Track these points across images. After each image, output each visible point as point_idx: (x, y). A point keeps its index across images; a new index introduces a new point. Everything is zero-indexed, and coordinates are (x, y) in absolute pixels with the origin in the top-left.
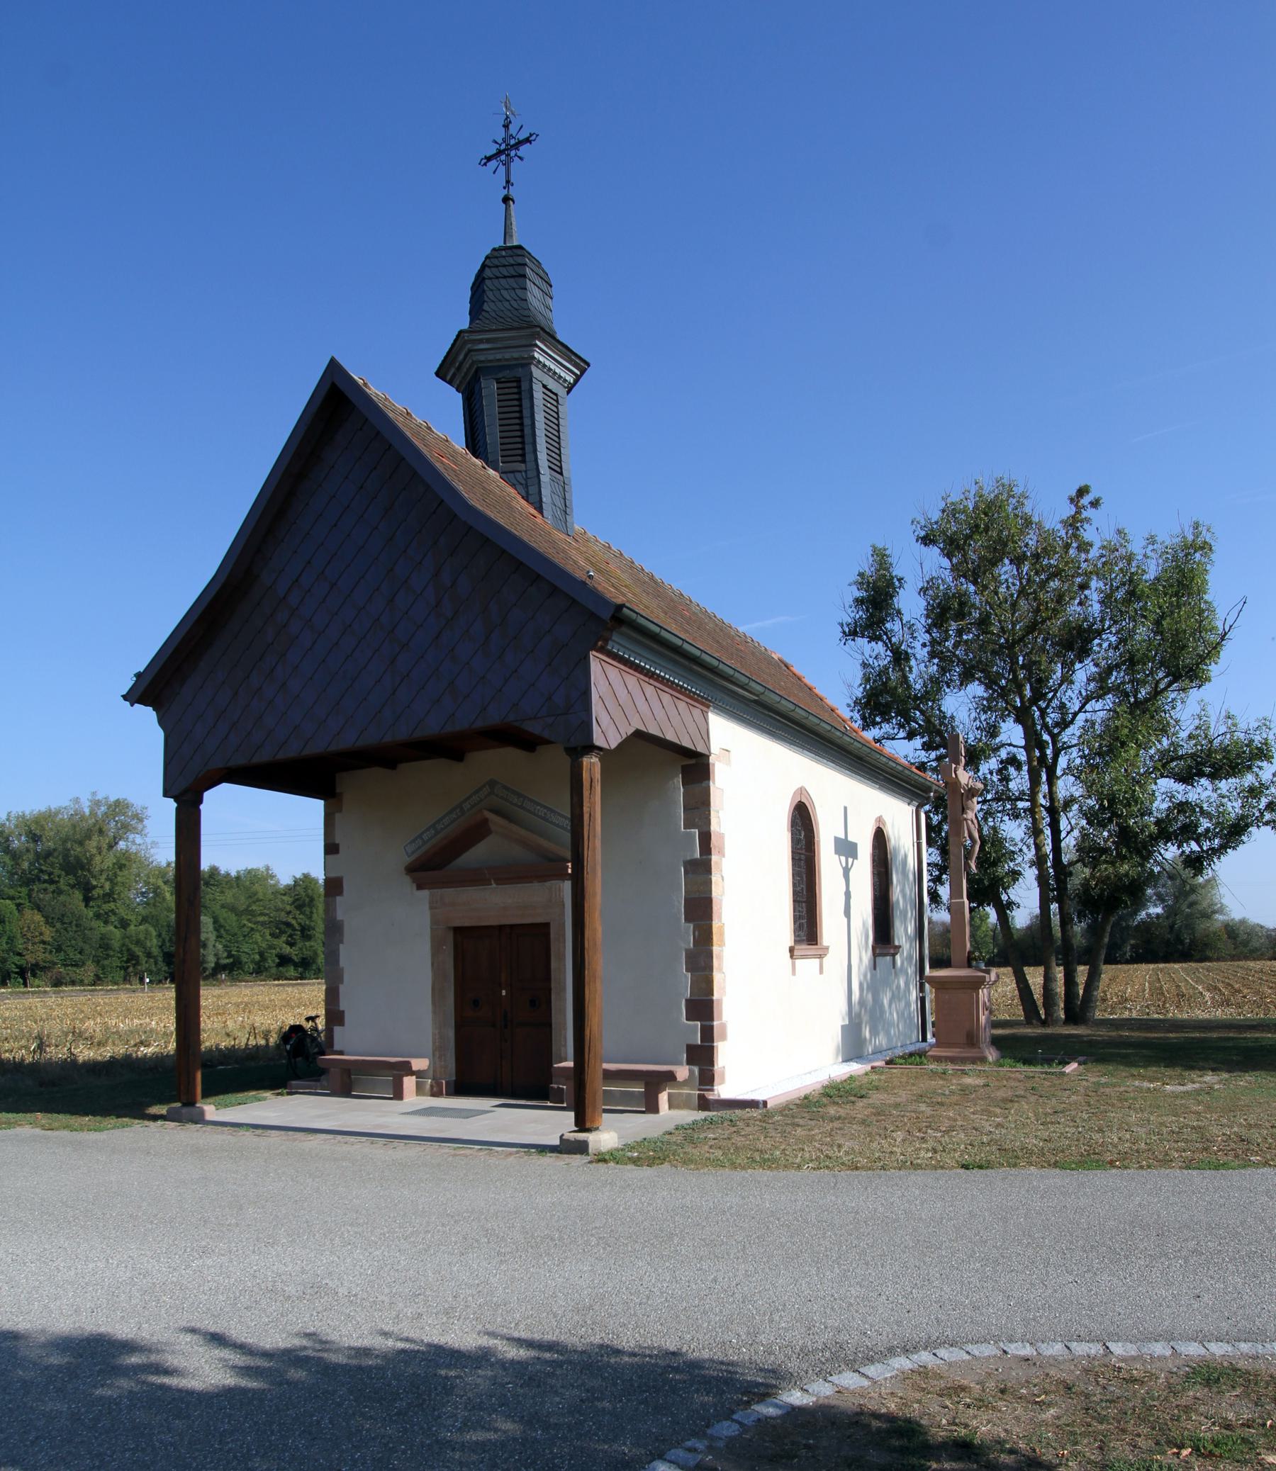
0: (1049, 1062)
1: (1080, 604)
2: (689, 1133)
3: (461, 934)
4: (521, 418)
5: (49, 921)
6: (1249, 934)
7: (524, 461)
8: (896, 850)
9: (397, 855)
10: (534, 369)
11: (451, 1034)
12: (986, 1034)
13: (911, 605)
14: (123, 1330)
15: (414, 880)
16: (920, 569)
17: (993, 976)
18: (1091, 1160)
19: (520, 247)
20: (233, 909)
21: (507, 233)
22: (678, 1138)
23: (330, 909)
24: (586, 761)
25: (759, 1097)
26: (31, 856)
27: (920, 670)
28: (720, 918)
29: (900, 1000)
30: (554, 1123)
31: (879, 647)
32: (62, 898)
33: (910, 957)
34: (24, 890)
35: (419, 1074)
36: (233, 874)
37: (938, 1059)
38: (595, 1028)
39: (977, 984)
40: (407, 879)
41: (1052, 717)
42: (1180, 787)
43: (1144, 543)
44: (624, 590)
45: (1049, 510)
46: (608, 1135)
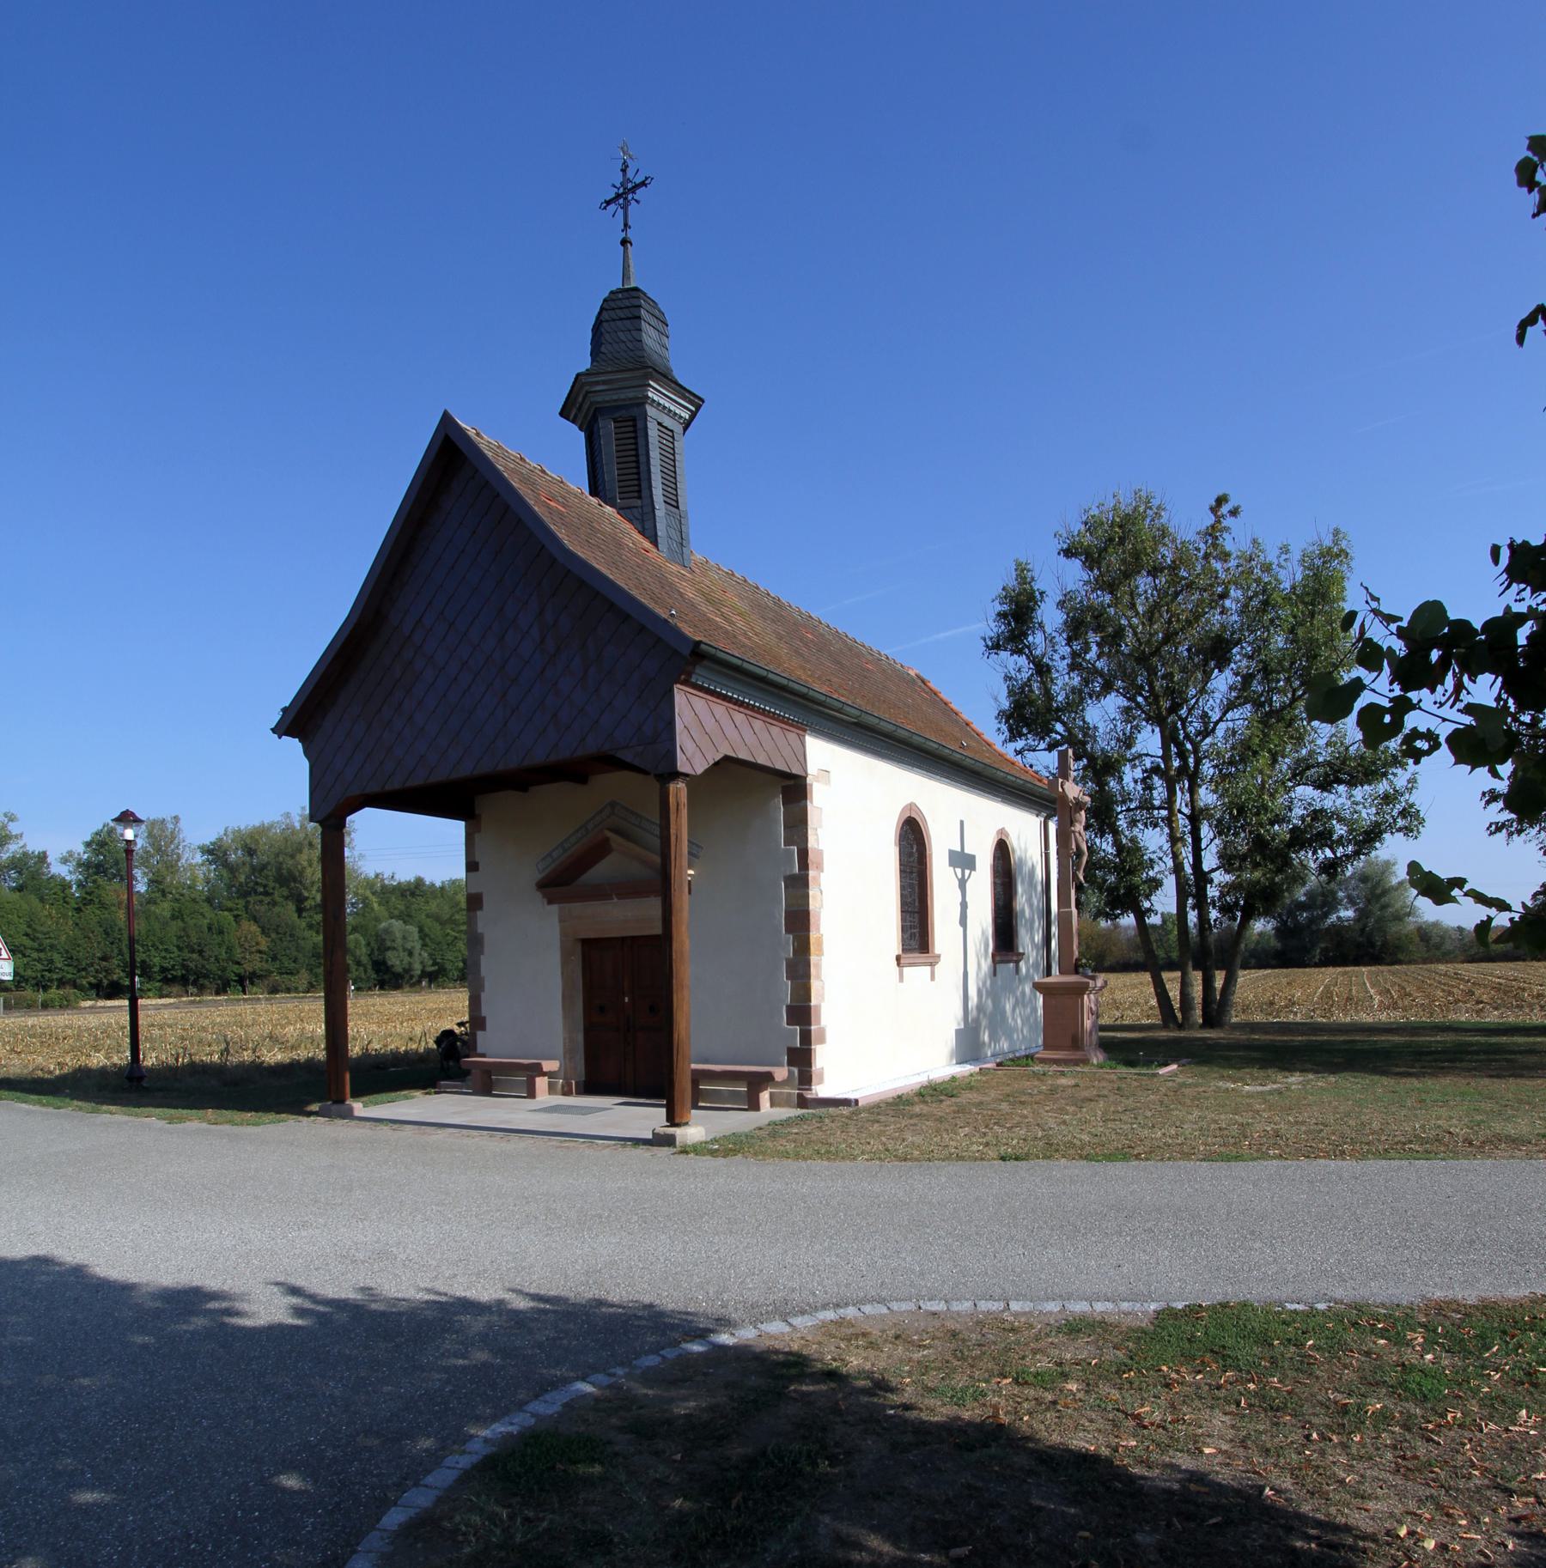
0: (1148, 1063)
1: (1222, 613)
2: (775, 1129)
3: (588, 944)
4: (637, 456)
6: (1442, 937)
7: (640, 497)
9: (530, 872)
10: (648, 408)
11: (580, 1037)
12: (1090, 1039)
14: (212, 1283)
15: (545, 896)
17: (1099, 983)
18: (1124, 1154)
19: (636, 289)
20: (437, 918)
21: (626, 276)
22: (762, 1133)
23: (471, 922)
24: (672, 787)
25: (852, 1096)
26: (247, 869)
27: (1063, 682)
28: (818, 929)
29: (1024, 1006)
30: (647, 1118)
32: (277, 909)
33: (1036, 965)
34: (242, 902)
35: (550, 1075)
36: (438, 884)
37: (1043, 1061)
38: (683, 1033)
39: (1081, 990)
40: (539, 895)
41: (1194, 726)
42: (1317, 793)
43: (1278, 552)
44: (735, 618)
45: (1186, 521)
46: (694, 1131)
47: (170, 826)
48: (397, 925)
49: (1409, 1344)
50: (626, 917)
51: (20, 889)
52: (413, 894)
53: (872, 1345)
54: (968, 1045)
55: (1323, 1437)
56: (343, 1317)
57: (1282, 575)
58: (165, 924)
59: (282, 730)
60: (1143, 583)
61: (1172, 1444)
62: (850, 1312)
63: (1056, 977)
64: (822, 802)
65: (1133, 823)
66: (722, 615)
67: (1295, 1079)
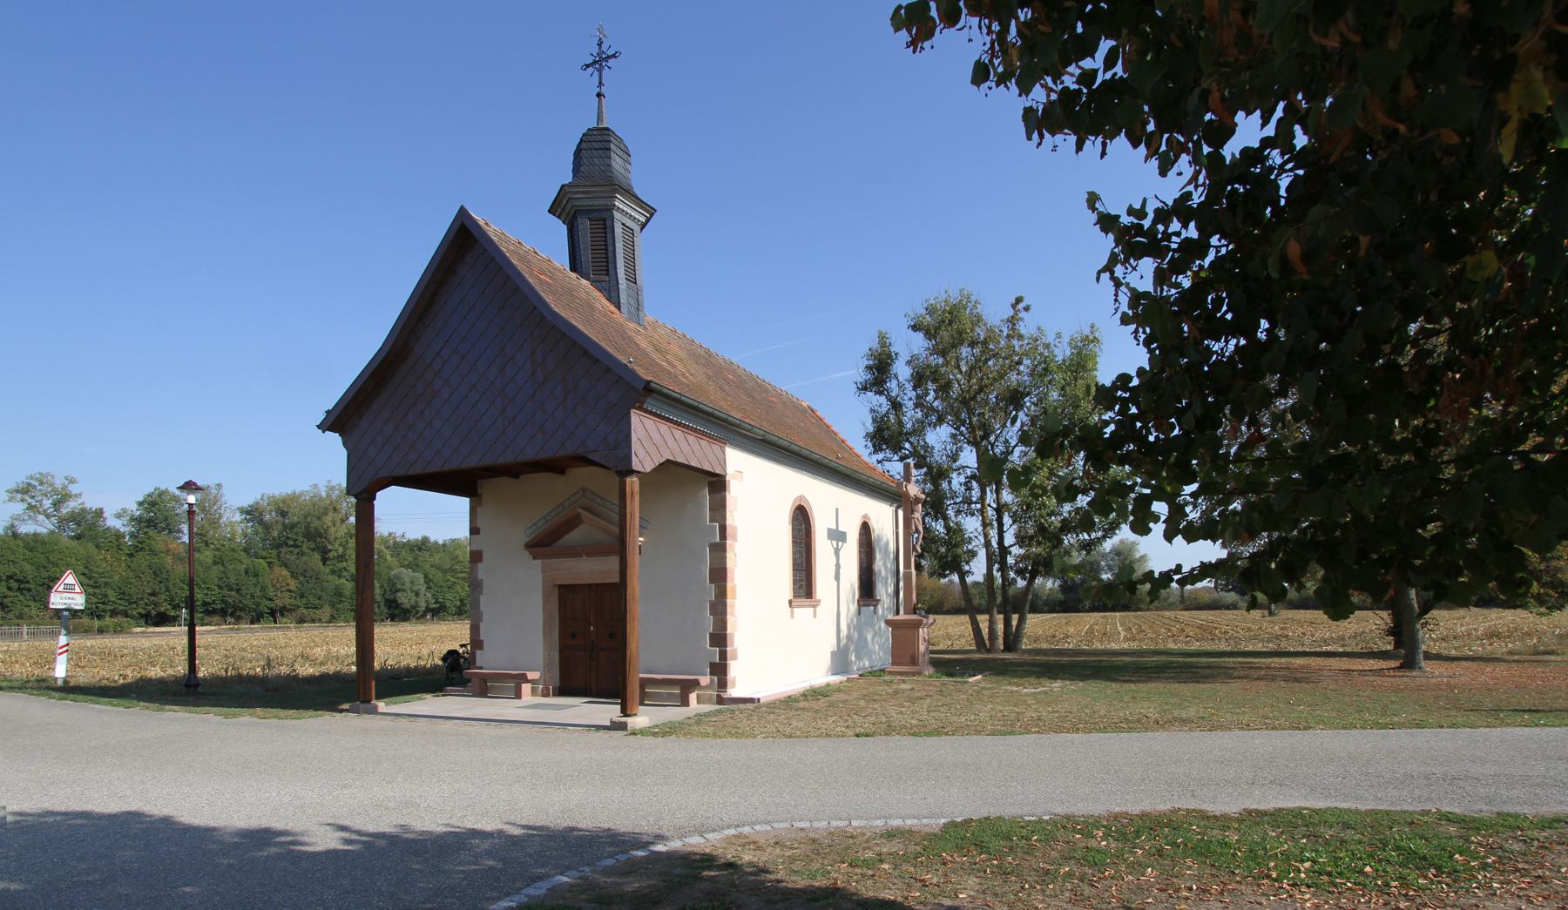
0: (962, 675)
2: (699, 719)
3: (564, 590)
5: (294, 575)
8: (880, 538)
11: (556, 656)
13: (902, 371)
14: (278, 824)
16: (910, 346)
18: (938, 732)
20: (439, 568)
23: (473, 571)
24: (628, 480)
27: (911, 415)
30: (608, 712)
31: (883, 399)
33: (889, 609)
34: (274, 552)
37: (891, 673)
39: (918, 625)
45: (994, 312)
46: (642, 718)
47: (214, 492)
48: (407, 574)
49: (1094, 837)
50: (597, 570)
51: (78, 537)
52: (420, 549)
53: (759, 848)
54: (840, 661)
55: (1032, 887)
56: (384, 842)
57: (1056, 352)
58: (208, 568)
59: (323, 427)
60: (965, 351)
61: (943, 894)
62: (746, 830)
63: (902, 616)
64: (736, 494)
65: (958, 512)
66: (667, 361)
67: (1057, 685)
